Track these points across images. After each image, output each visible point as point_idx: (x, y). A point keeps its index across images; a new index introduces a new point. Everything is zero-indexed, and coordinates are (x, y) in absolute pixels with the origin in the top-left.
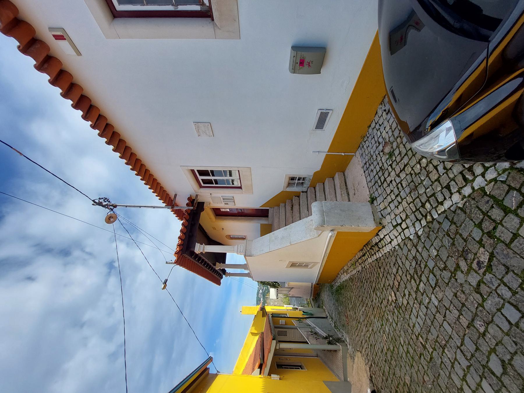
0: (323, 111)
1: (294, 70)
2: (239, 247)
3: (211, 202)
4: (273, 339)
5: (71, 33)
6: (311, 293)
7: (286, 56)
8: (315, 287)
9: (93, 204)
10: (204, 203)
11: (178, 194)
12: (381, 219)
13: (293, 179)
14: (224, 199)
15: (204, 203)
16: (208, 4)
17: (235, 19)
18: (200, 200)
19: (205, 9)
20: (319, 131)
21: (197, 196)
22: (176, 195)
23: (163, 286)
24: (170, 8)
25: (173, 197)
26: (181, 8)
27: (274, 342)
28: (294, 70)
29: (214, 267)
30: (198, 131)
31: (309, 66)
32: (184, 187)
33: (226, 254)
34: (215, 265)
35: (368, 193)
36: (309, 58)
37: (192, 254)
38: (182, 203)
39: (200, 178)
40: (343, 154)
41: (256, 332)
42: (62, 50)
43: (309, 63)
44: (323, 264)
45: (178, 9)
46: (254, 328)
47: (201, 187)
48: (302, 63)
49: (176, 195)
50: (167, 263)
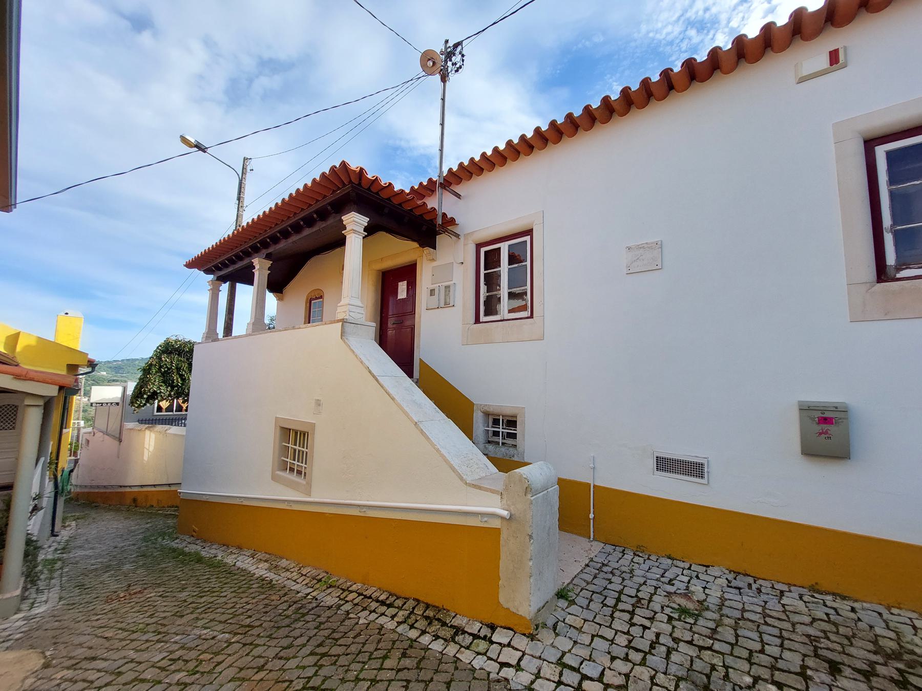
0: (706, 466)
1: (806, 409)
2: (359, 310)
3: (435, 264)
4: (61, 388)
5: (837, 76)
6: (98, 487)
7: (825, 394)
8: (123, 494)
9: (447, 42)
10: (434, 247)
11: (460, 202)
12: (545, 625)
13: (512, 423)
14: (447, 287)
15: (434, 247)
16: (898, 276)
17: (888, 315)
18: (441, 240)
19: (891, 272)
20: (652, 463)
21: (457, 236)
22: (458, 196)
23: (193, 141)
24: (887, 220)
25: (457, 189)
26: (889, 239)
27: (53, 391)
28: (806, 409)
29: (265, 252)
30: (639, 247)
31: (821, 434)
32: (481, 212)
33: (252, 284)
34: (268, 257)
35: (567, 582)
36: (827, 434)
37: (340, 206)
38: (443, 204)
39: (504, 247)
40: (591, 516)
41: (19, 348)
42: (812, 56)
43: (826, 433)
44: (296, 507)
45: (885, 233)
46: (33, 342)
47: (479, 246)
48: (825, 421)
49: (458, 196)
50: (245, 159)
